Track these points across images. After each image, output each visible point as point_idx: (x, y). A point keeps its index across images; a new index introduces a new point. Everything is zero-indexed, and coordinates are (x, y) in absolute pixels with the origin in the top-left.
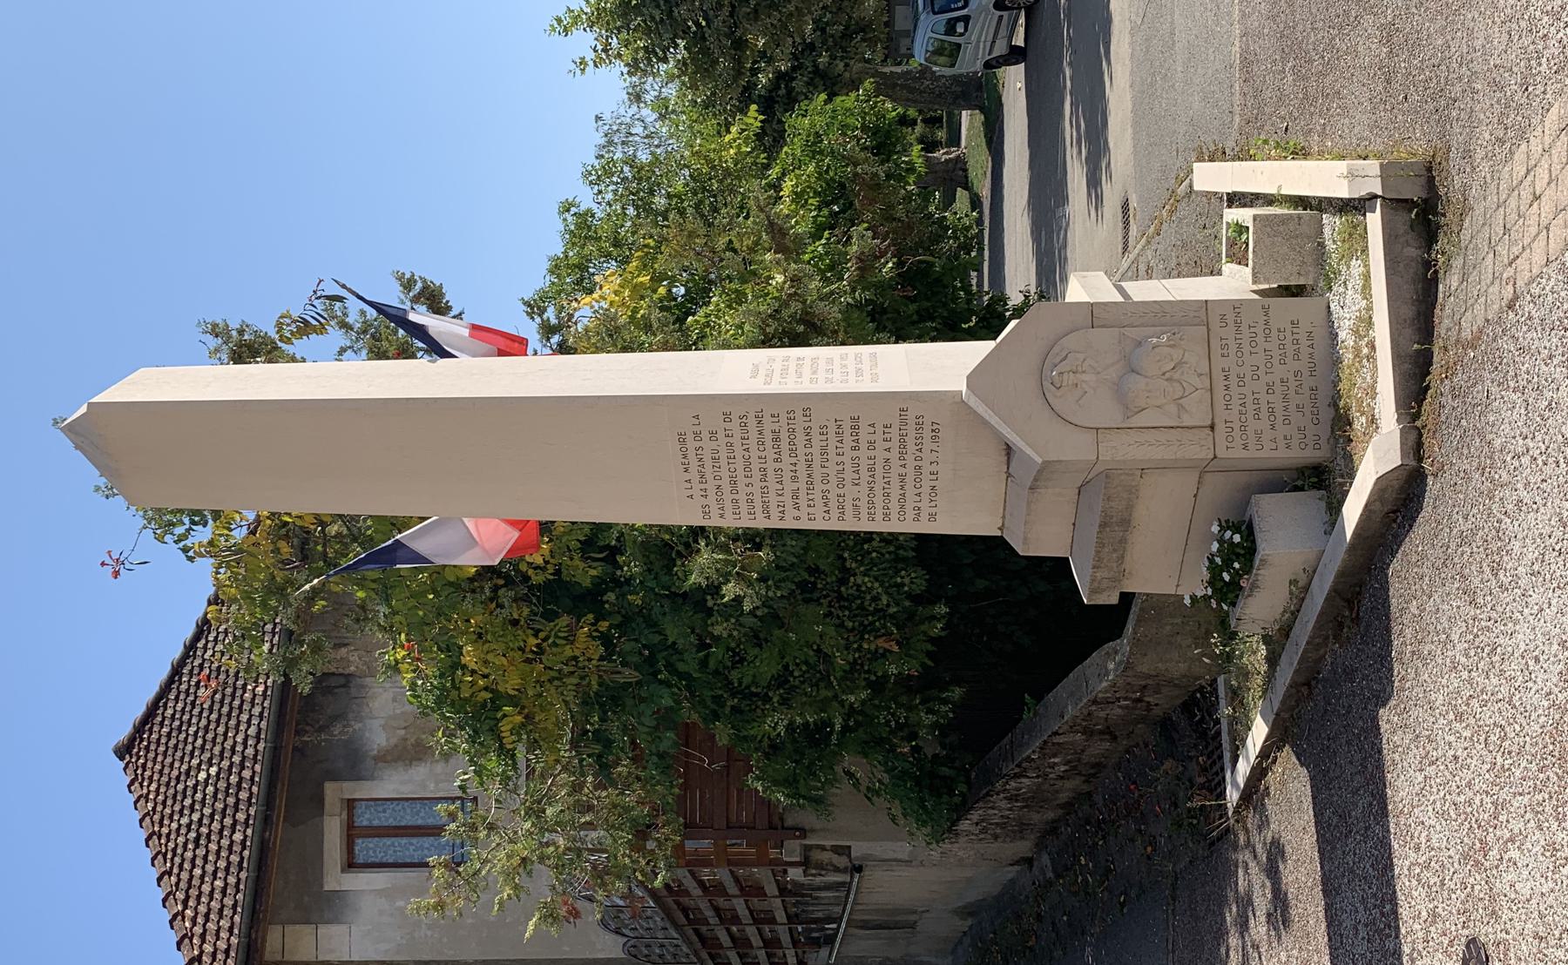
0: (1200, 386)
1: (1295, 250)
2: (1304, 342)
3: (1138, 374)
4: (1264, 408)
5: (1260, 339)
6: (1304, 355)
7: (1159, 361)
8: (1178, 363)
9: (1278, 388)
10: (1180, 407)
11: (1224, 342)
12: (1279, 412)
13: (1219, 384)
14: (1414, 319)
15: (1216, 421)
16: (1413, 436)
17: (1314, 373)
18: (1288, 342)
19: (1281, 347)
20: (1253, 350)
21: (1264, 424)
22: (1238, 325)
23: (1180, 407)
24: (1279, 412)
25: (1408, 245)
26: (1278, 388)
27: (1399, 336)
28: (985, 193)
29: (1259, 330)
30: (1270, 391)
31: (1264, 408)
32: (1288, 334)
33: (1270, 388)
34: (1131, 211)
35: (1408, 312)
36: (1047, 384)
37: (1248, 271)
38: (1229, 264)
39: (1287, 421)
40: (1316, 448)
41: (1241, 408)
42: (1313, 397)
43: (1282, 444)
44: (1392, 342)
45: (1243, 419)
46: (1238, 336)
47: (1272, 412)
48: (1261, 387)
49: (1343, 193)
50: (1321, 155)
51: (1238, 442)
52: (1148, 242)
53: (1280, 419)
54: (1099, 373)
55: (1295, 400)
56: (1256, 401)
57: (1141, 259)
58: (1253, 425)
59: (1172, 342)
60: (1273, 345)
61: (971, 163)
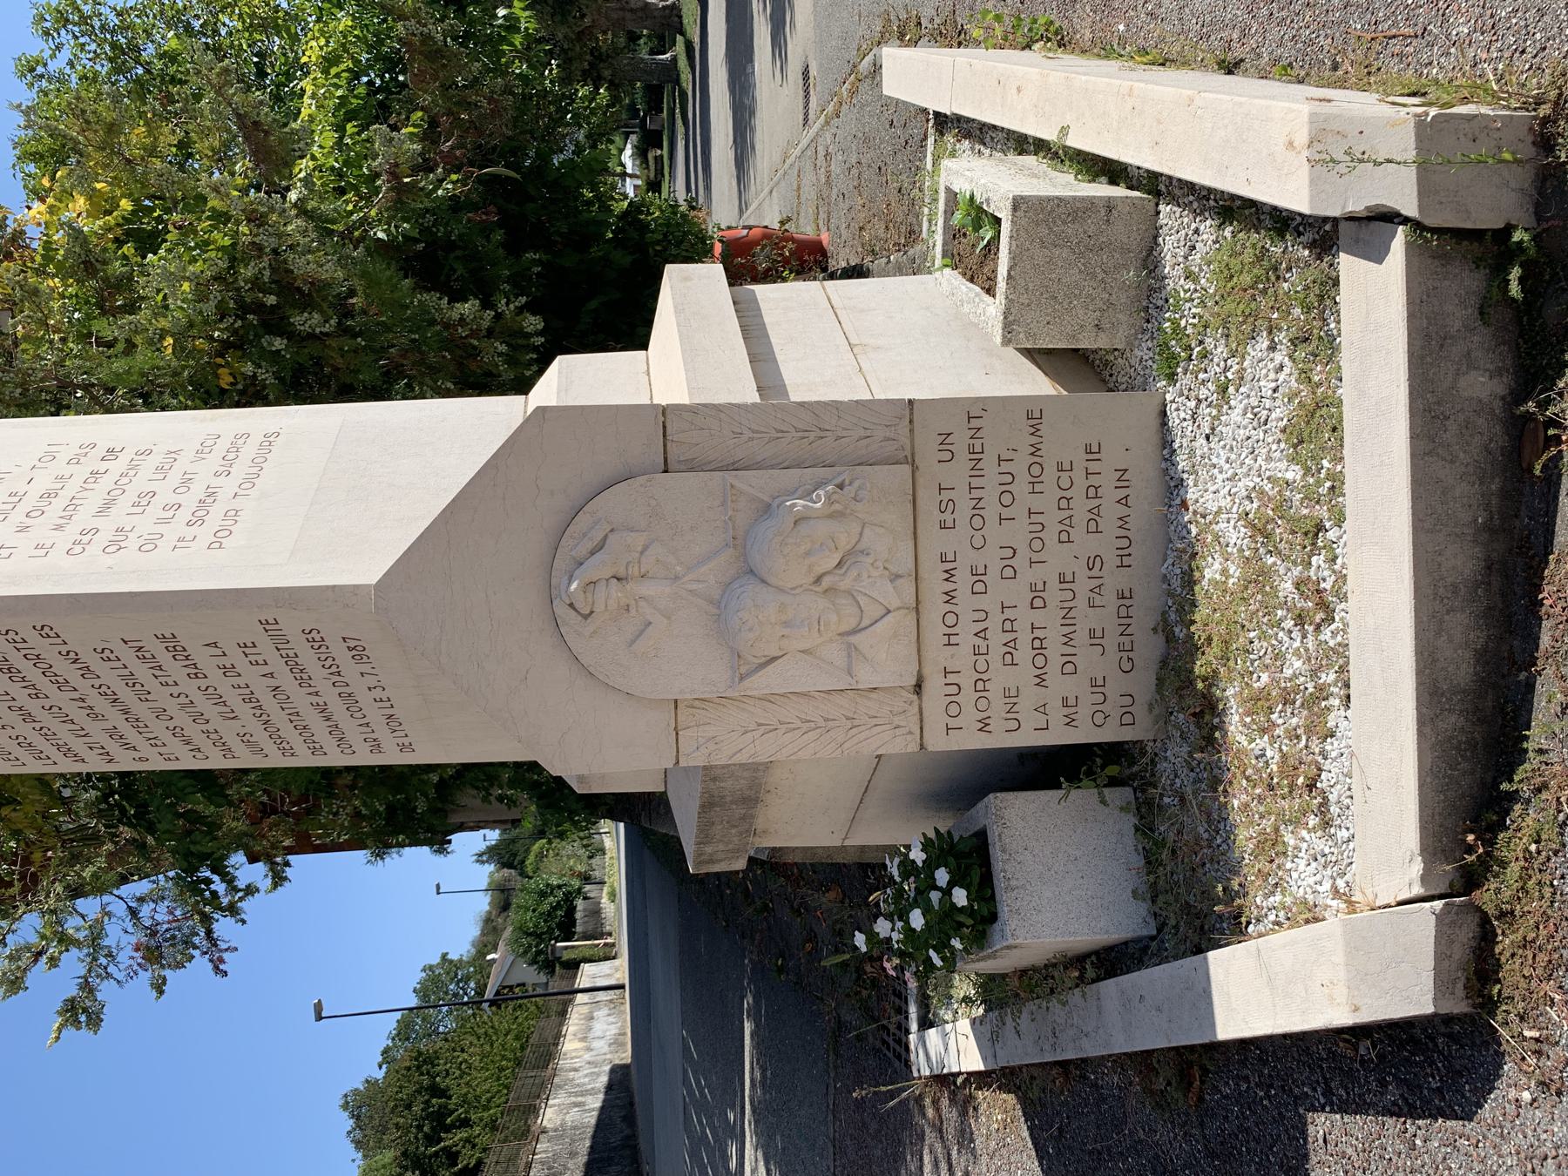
0: (894, 603)
1: (1094, 276)
2: (1110, 494)
3: (763, 581)
4: (1024, 638)
5: (1021, 487)
6: (1109, 523)
7: (808, 554)
8: (850, 553)
9: (1054, 595)
10: (852, 649)
11: (946, 495)
12: (1054, 649)
13: (934, 584)
14: (1477, 585)
15: (926, 672)
16: (1467, 932)
17: (1126, 561)
18: (1077, 493)
19: (1064, 503)
20: (1006, 513)
21: (1024, 674)
22: (976, 455)
23: (852, 649)
24: (1054, 649)
25: (1472, 366)
26: (1054, 595)
27: (1438, 634)
28: (697, 40)
29: (1020, 466)
30: (1038, 603)
31: (1024, 638)
32: (1078, 475)
33: (1037, 596)
34: (811, 80)
35: (1463, 561)
36: (561, 610)
37: (993, 308)
38: (947, 271)
39: (1069, 666)
40: (1130, 722)
41: (979, 641)
42: (1123, 611)
43: (1057, 715)
44: (1419, 652)
45: (981, 666)
46: (975, 482)
47: (1039, 647)
48: (1018, 592)
49: (1294, 195)
50: (1105, 49)
51: (970, 717)
52: (827, 123)
53: (1056, 661)
54: (677, 578)
55: (1086, 620)
56: (1009, 626)
57: (820, 140)
58: (1000, 678)
59: (837, 507)
60: (1047, 502)
61: (684, 11)
